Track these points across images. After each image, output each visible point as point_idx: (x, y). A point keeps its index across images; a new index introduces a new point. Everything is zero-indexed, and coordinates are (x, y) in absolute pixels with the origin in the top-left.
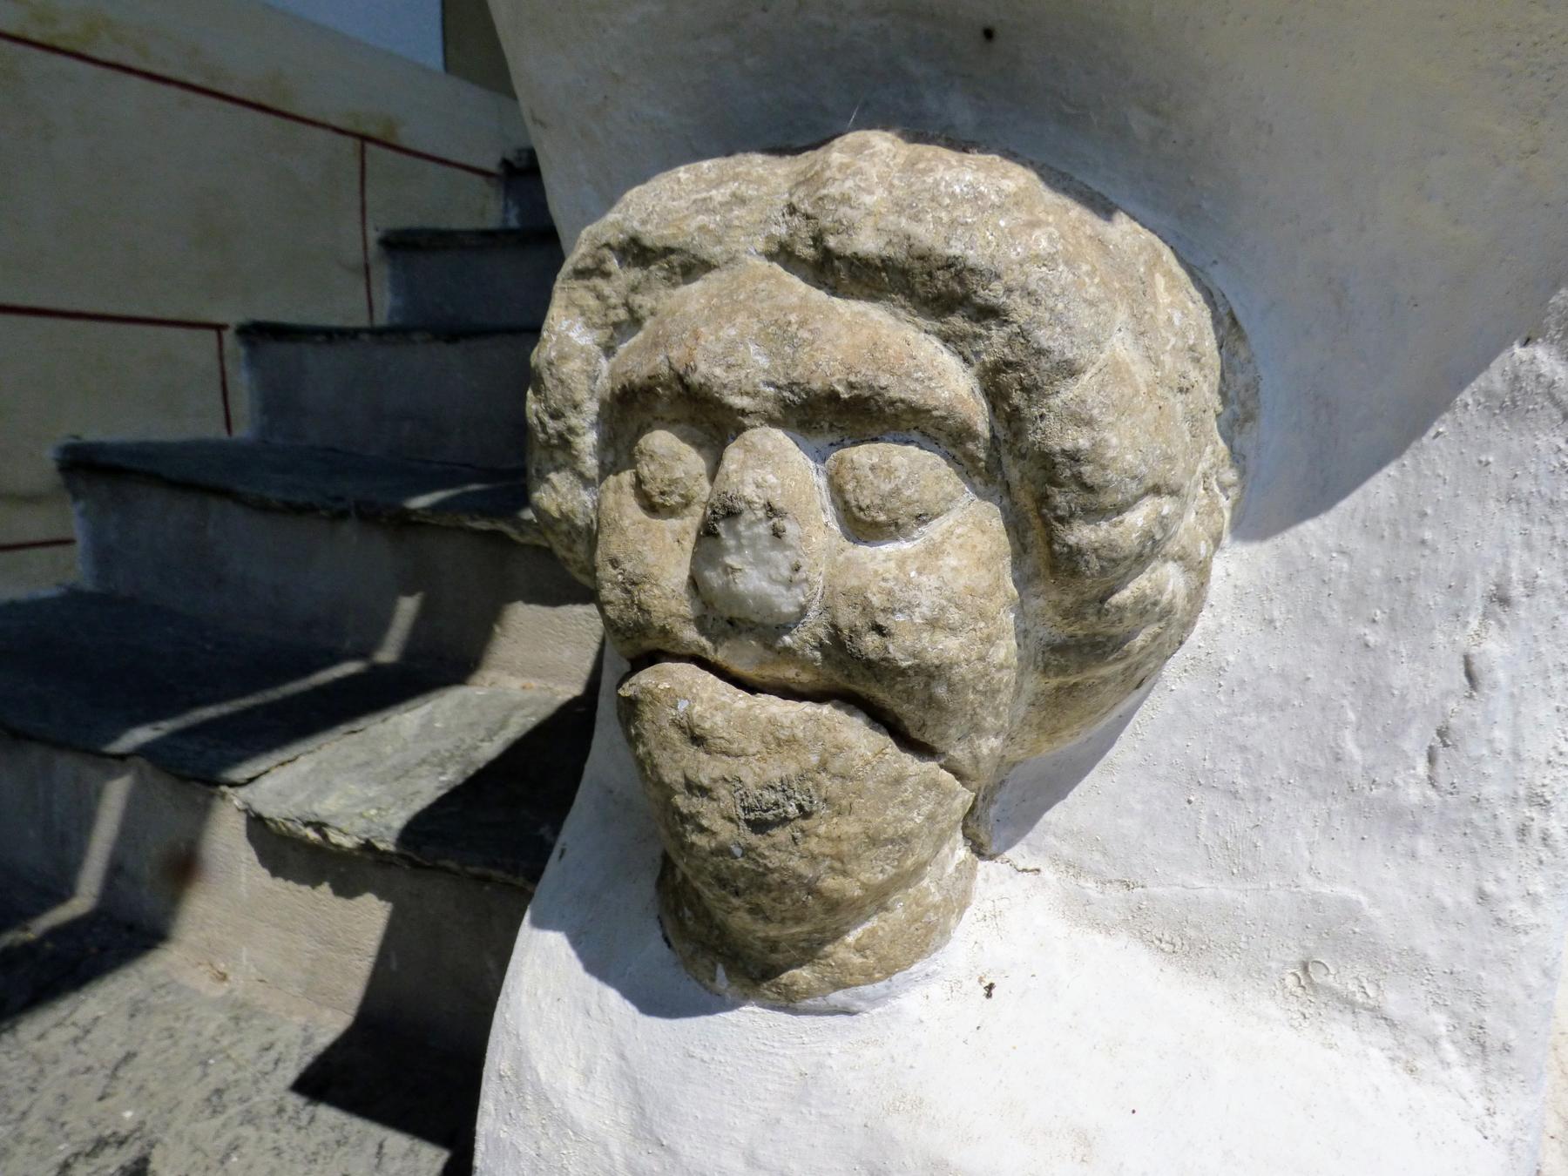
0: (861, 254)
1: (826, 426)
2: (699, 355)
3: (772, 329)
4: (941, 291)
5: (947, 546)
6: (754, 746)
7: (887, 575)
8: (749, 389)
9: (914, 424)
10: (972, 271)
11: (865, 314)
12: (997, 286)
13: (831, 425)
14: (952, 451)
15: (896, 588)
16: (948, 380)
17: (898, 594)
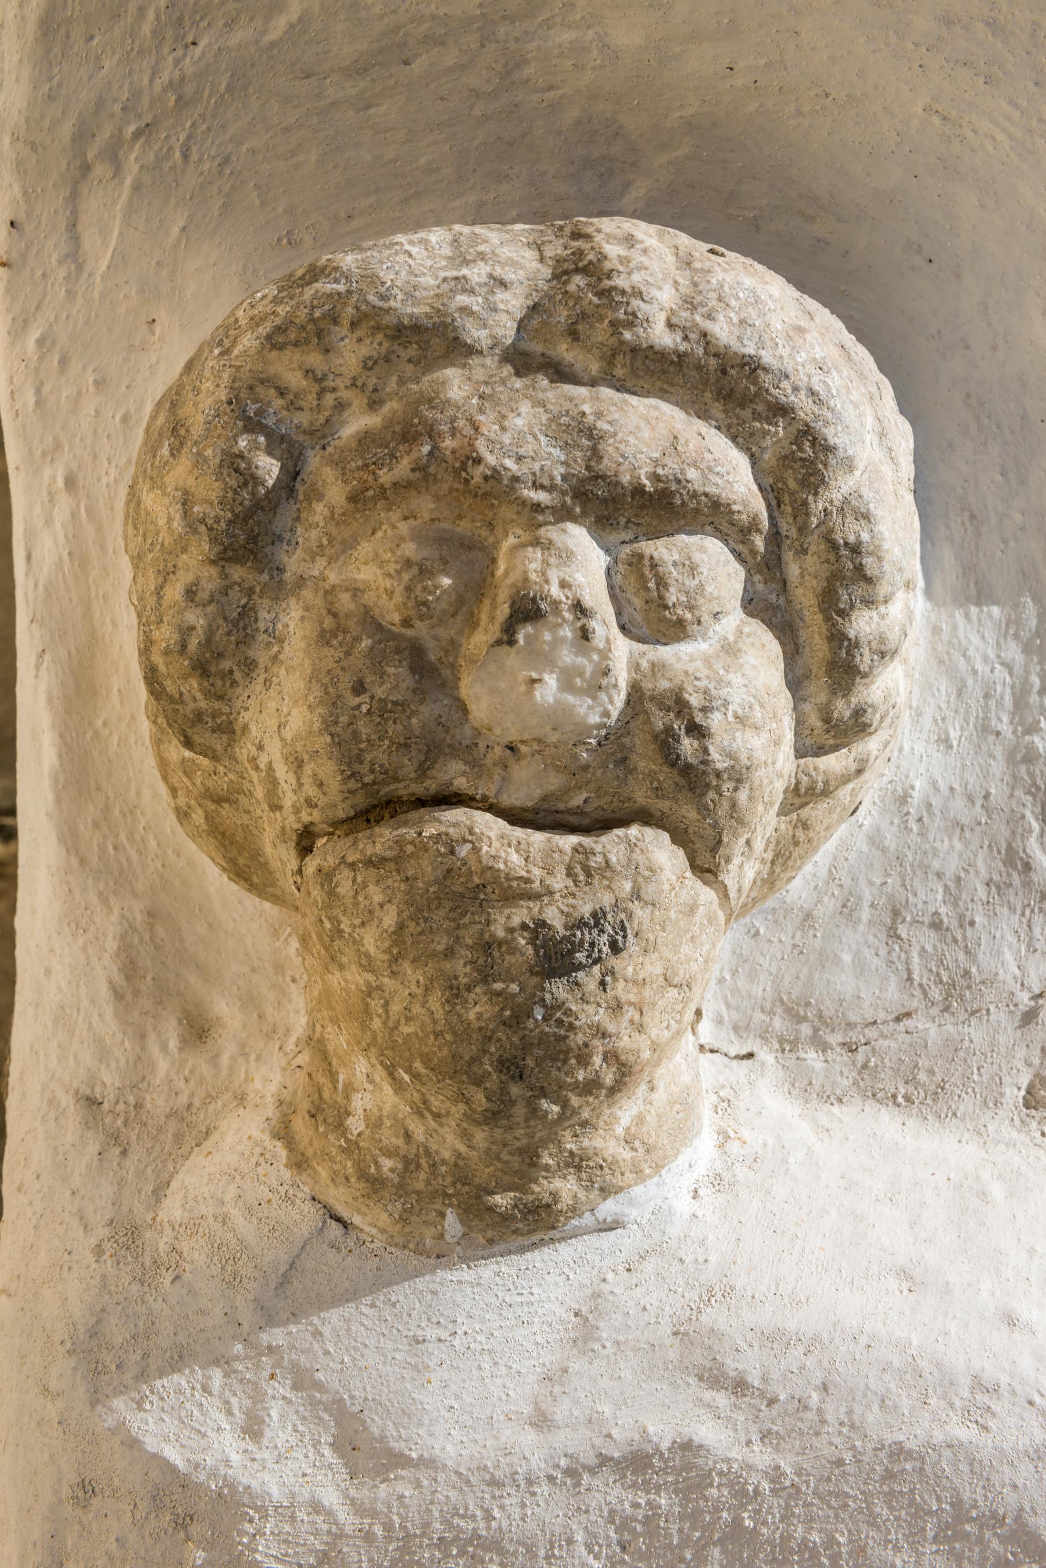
0: (657, 348)
1: (623, 521)
2: (481, 445)
3: (564, 420)
4: (728, 386)
5: (741, 645)
6: (559, 882)
7: (698, 674)
8: (546, 482)
9: (711, 519)
10: (764, 369)
11: (656, 408)
12: (785, 384)
13: (629, 521)
14: (740, 547)
15: (711, 686)
16: (732, 474)
17: (714, 692)
